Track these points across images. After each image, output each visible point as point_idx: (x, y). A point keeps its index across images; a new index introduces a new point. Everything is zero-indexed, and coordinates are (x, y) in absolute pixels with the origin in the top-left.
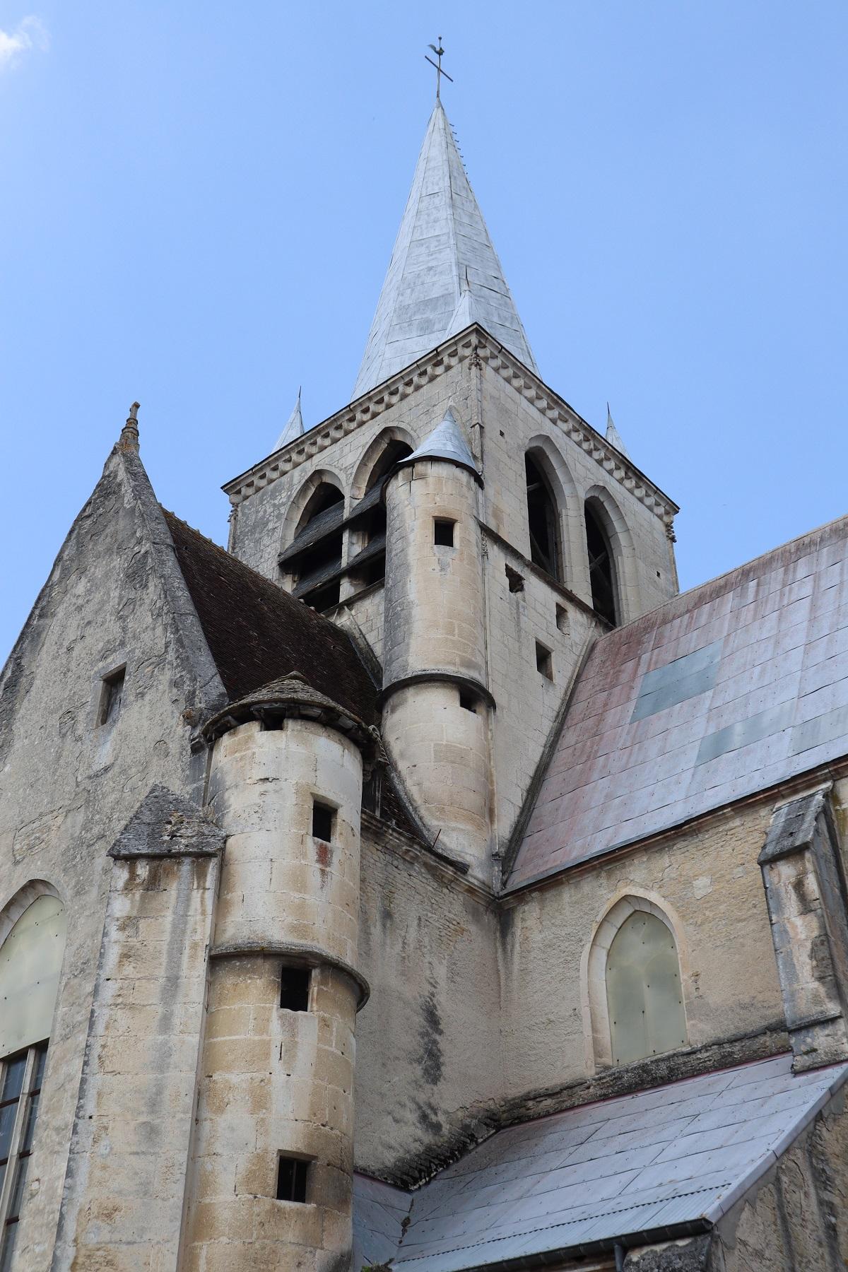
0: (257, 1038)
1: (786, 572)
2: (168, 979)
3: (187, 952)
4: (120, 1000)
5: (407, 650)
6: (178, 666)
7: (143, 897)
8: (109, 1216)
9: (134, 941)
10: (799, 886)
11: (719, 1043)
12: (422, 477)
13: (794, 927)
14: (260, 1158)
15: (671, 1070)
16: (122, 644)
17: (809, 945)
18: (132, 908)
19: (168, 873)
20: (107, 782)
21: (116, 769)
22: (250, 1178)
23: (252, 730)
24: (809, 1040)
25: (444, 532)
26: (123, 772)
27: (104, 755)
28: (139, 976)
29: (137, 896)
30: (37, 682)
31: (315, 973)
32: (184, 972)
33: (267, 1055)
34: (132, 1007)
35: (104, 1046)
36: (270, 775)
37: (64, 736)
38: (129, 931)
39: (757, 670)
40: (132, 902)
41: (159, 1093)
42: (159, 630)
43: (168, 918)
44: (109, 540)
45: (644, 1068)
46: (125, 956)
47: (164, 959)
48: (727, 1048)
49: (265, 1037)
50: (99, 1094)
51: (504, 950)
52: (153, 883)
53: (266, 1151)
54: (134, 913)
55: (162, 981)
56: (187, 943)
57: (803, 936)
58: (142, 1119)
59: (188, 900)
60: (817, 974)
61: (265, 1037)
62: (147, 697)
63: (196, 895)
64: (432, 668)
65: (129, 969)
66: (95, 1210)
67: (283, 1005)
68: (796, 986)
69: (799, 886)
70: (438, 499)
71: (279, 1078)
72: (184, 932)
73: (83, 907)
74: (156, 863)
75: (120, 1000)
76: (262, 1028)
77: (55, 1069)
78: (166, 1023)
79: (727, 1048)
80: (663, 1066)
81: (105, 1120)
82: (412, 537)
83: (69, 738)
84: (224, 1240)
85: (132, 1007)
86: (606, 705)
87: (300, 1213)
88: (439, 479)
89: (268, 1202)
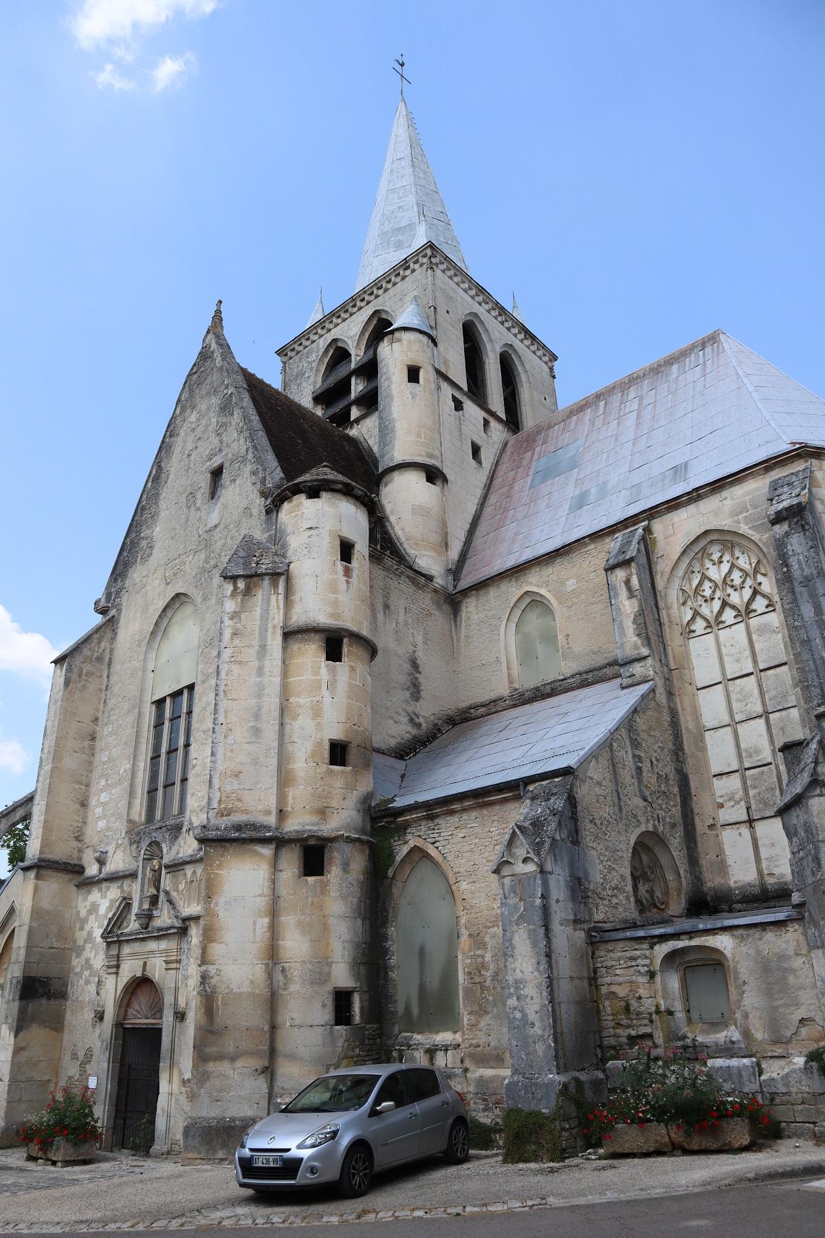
0: (314, 678)
1: (622, 396)
2: (260, 646)
3: (270, 631)
4: (233, 659)
5: (393, 448)
6: (254, 462)
7: (242, 600)
8: (236, 776)
9: (238, 625)
10: (627, 582)
11: (580, 674)
12: (399, 340)
13: (624, 606)
14: (319, 744)
15: (552, 689)
16: (220, 450)
17: (632, 616)
18: (236, 607)
19: (256, 586)
20: (217, 534)
21: (222, 526)
22: (314, 754)
23: (301, 499)
24: (631, 670)
25: (413, 374)
26: (226, 527)
27: (214, 518)
28: (243, 645)
29: (239, 600)
30: (171, 476)
31: (345, 640)
32: (269, 642)
33: (320, 688)
34: (240, 663)
35: (226, 685)
36: (314, 526)
37: (189, 507)
38: (236, 620)
39: (605, 456)
40: (236, 603)
41: (259, 710)
42: (242, 441)
43: (258, 612)
44: (208, 386)
45: (537, 689)
46: (234, 634)
47: (257, 635)
48: (585, 676)
49: (318, 677)
50: (226, 711)
51: (456, 625)
52: (248, 592)
53: (322, 740)
54: (238, 609)
55: (257, 647)
56: (270, 626)
57: (629, 612)
58: (251, 724)
59: (269, 600)
60: (636, 633)
61: (318, 677)
62: (237, 482)
63: (273, 598)
64: (409, 459)
65: (237, 642)
66: (229, 773)
67: (328, 659)
68: (624, 640)
69: (627, 582)
70: (409, 354)
71: (327, 700)
72: (267, 619)
73: (208, 608)
74: (248, 580)
75: (233, 659)
76: (316, 673)
77: (200, 700)
78: (260, 671)
79: (585, 676)
80: (548, 687)
81: (230, 725)
82: (394, 378)
83: (192, 509)
84: (302, 787)
85: (240, 663)
86: (514, 479)
87: (343, 772)
88: (410, 341)
89: (325, 767)
